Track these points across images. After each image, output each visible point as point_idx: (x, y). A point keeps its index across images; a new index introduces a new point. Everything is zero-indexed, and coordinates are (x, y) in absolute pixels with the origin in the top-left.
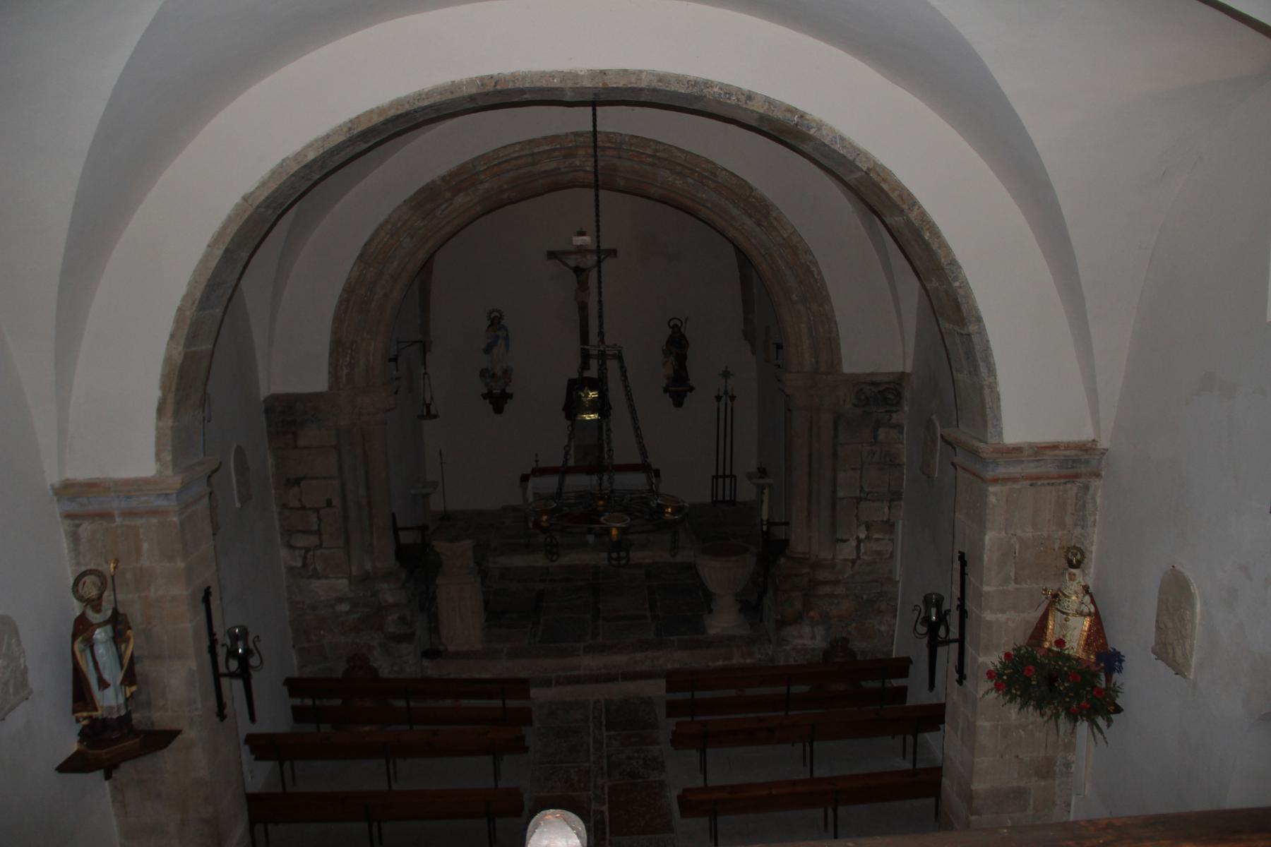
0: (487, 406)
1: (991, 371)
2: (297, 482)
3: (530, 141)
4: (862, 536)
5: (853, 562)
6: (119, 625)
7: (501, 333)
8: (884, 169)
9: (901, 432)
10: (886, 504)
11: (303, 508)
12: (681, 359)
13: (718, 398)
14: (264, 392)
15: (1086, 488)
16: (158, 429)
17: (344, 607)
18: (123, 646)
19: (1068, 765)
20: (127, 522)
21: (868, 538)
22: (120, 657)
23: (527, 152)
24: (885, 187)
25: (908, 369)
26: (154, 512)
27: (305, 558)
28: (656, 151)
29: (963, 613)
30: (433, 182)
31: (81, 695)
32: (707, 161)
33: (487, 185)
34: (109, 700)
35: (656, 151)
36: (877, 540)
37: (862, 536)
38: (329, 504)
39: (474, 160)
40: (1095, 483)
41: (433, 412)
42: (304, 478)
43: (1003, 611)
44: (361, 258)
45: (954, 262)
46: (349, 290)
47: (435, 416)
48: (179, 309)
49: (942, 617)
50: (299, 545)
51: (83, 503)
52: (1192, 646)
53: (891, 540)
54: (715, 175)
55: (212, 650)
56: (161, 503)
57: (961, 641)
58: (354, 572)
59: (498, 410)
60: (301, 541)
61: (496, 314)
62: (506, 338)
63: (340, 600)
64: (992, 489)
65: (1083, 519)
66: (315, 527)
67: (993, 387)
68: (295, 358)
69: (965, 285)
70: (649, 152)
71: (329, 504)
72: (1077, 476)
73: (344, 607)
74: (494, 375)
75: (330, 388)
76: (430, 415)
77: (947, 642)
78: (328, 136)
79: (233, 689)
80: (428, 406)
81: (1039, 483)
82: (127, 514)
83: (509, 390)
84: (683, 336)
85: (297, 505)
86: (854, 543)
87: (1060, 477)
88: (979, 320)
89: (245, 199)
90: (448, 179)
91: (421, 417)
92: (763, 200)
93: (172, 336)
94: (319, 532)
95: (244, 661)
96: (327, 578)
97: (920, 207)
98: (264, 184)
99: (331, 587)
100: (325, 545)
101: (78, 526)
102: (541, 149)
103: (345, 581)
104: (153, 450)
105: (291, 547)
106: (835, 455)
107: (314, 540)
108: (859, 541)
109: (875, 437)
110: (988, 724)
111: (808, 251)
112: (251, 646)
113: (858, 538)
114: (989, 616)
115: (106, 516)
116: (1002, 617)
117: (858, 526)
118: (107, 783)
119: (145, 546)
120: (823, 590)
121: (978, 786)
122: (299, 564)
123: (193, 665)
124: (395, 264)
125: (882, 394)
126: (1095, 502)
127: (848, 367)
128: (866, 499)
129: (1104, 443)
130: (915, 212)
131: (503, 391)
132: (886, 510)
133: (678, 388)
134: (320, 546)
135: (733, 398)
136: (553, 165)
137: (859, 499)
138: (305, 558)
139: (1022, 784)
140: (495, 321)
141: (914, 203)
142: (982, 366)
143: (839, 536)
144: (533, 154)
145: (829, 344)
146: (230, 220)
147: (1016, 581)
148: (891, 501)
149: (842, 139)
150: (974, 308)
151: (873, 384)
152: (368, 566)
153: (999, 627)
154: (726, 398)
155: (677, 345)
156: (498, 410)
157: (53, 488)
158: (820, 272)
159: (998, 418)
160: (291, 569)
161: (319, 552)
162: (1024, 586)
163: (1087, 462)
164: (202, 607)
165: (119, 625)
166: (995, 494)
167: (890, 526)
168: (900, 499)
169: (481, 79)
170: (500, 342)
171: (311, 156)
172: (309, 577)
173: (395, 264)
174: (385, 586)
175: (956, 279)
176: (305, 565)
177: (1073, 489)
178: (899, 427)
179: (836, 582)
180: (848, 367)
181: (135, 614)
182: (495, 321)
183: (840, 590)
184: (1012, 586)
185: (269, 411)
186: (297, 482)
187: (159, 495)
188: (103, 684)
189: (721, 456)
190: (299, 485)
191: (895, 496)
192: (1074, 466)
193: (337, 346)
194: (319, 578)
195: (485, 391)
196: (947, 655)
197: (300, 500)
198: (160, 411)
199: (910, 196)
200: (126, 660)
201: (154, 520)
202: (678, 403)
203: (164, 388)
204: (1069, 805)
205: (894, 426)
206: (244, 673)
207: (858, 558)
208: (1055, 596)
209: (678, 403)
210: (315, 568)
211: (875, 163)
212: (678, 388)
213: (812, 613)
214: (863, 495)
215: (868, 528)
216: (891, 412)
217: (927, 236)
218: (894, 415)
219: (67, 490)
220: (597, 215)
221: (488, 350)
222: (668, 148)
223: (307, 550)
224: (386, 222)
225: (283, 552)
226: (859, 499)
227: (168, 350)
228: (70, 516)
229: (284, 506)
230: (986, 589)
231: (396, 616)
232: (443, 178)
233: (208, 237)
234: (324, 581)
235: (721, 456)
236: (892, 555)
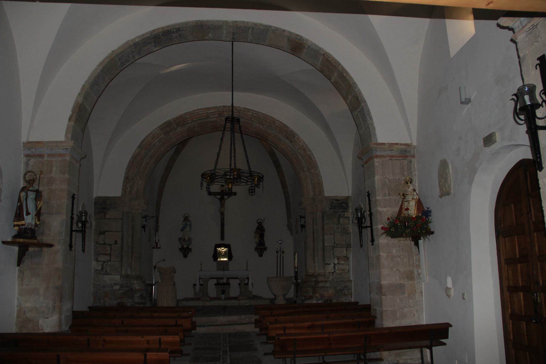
0: (181, 255)
1: (371, 118)
2: (104, 233)
3: (206, 108)
4: (336, 262)
5: (333, 273)
6: (38, 195)
7: (188, 223)
8: (329, 54)
9: (349, 220)
10: (345, 249)
11: (105, 244)
12: (262, 236)
13: (277, 252)
14: (95, 195)
15: (411, 162)
16: (68, 126)
17: (117, 287)
18: (38, 203)
19: (419, 274)
20: (49, 159)
21: (338, 263)
22: (36, 207)
23: (205, 112)
24: (330, 59)
25: (350, 195)
26: (60, 155)
27: (103, 265)
28: (253, 114)
29: (371, 215)
30: (170, 120)
31: (19, 216)
32: (272, 118)
33: (189, 125)
34: (29, 220)
35: (253, 114)
36: (342, 264)
37: (336, 262)
38: (116, 242)
39: (185, 114)
40: (414, 160)
41: (159, 246)
42: (107, 231)
43: (385, 207)
44: (139, 147)
45: (354, 83)
46: (134, 158)
47: (160, 248)
48: (83, 85)
49: (363, 216)
50: (101, 260)
51: (33, 150)
52: (450, 180)
53: (348, 264)
54: (274, 123)
55: (72, 218)
56: (64, 152)
57: (371, 227)
58: (123, 273)
59: (185, 256)
60: (102, 258)
61: (187, 215)
62: (190, 226)
63: (116, 284)
64: (376, 160)
65: (411, 173)
66: (109, 252)
67: (372, 124)
68: (109, 183)
69: (359, 90)
70: (250, 114)
71: (116, 242)
72: (406, 157)
73: (117, 287)
74: (184, 239)
75: (122, 195)
76: (157, 247)
77: (367, 227)
78: (144, 35)
79: (77, 238)
80: (157, 244)
81: (393, 158)
82: (49, 155)
83: (190, 247)
84: (262, 227)
85: (102, 242)
86: (333, 265)
87: (400, 157)
88: (365, 102)
89: (113, 52)
90: (175, 120)
91: (154, 248)
92: (292, 132)
93: (79, 94)
94: (110, 254)
95: (84, 223)
96: (111, 275)
97: (342, 66)
98: (120, 48)
99: (113, 279)
100: (112, 260)
101: (29, 160)
102: (211, 111)
103: (119, 276)
104: (64, 133)
105: (97, 260)
106: (323, 229)
107: (108, 258)
108: (335, 265)
109: (339, 222)
110: (385, 255)
111: (310, 150)
112: (88, 219)
113: (334, 263)
114: (380, 209)
115: (41, 156)
116: (385, 210)
117: (334, 258)
118: (17, 268)
119: (54, 169)
120: (321, 285)
121: (384, 282)
122: (100, 268)
123: (64, 217)
124: (152, 151)
125: (341, 204)
126: (414, 168)
127: (327, 194)
128: (336, 247)
129: (415, 143)
130: (340, 67)
131: (188, 247)
132: (345, 251)
133: (261, 248)
134: (110, 261)
135: (283, 252)
136: (215, 119)
137: (334, 247)
138: (103, 265)
139: (402, 282)
140: (186, 219)
141: (339, 64)
142: (368, 117)
143: (326, 262)
144: (207, 113)
145: (318, 185)
146: (106, 58)
147: (389, 196)
148: (347, 248)
149: (314, 44)
150: (363, 97)
151: (336, 200)
152: (129, 273)
153: (385, 211)
154: (280, 252)
155: (260, 230)
156: (185, 256)
157: (23, 143)
158: (314, 158)
159: (375, 135)
160: (96, 270)
161: (109, 263)
162: (392, 197)
163: (410, 152)
164: (71, 200)
165: (38, 195)
166: (377, 162)
167: (347, 258)
168: (350, 247)
169: (196, 21)
170: (188, 226)
171: (137, 40)
172: (104, 274)
173: (152, 151)
174: (136, 282)
175: (356, 88)
176: (102, 268)
177: (406, 162)
178: (348, 218)
179: (326, 281)
180: (327, 194)
181: (45, 195)
182: (186, 219)
183: (328, 285)
184: (387, 197)
185: (96, 203)
186: (104, 233)
187: (64, 149)
188: (28, 214)
189: (279, 260)
190: (104, 234)
191: (348, 246)
192: (405, 153)
193: (127, 179)
194: (108, 275)
195: (180, 247)
196: (367, 232)
197: (104, 240)
198: (70, 119)
199: (338, 62)
200: (38, 208)
201: (60, 159)
202: (261, 255)
203: (73, 111)
204: (422, 293)
205: (346, 218)
206: (83, 231)
207: (335, 272)
208: (403, 195)
209: (261, 255)
210: (106, 270)
211: (326, 52)
212: (261, 248)
213: (317, 295)
214: (335, 245)
215: (338, 259)
216: (345, 211)
217: (345, 74)
218: (346, 213)
219: (29, 145)
220: (232, 71)
221: (182, 230)
222: (257, 112)
223: (104, 262)
224: (151, 133)
225: (94, 263)
226: (334, 247)
227: (77, 98)
228: (27, 156)
229: (97, 243)
230: (378, 198)
231: (139, 295)
232: (173, 119)
233: (97, 63)
234: (109, 276)
235: (279, 260)
236: (348, 271)
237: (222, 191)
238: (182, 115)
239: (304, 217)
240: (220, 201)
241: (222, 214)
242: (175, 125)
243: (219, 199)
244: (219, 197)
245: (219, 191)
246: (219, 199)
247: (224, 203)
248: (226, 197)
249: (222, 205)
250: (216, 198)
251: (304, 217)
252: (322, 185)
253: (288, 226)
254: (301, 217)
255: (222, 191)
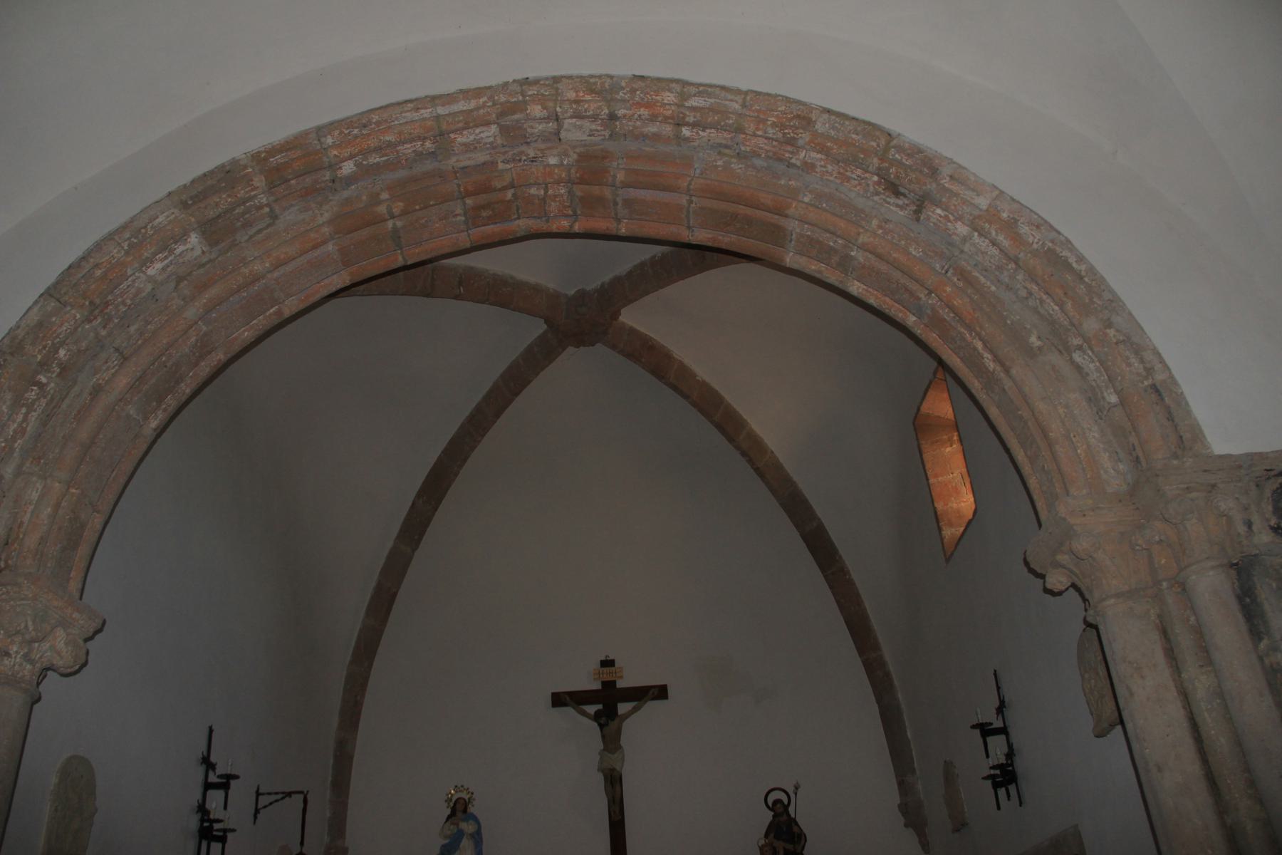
7: (469, 827)
30: (234, 162)
32: (788, 100)
44: (49, 293)
61: (465, 795)
62: (477, 837)
136: (481, 157)
140: (459, 809)
144: (438, 117)
158: (1081, 259)
170: (466, 844)
237: (605, 684)
238: (305, 134)
239: (1003, 731)
240: (601, 726)
241: (613, 781)
242: (259, 181)
243: (596, 717)
244: (592, 709)
245: (597, 686)
246: (596, 717)
247: (619, 732)
248: (623, 708)
249: (612, 743)
250: (584, 714)
251: (1003, 731)
252: (1180, 399)
253: (904, 809)
254: (986, 731)
255: (605, 684)
